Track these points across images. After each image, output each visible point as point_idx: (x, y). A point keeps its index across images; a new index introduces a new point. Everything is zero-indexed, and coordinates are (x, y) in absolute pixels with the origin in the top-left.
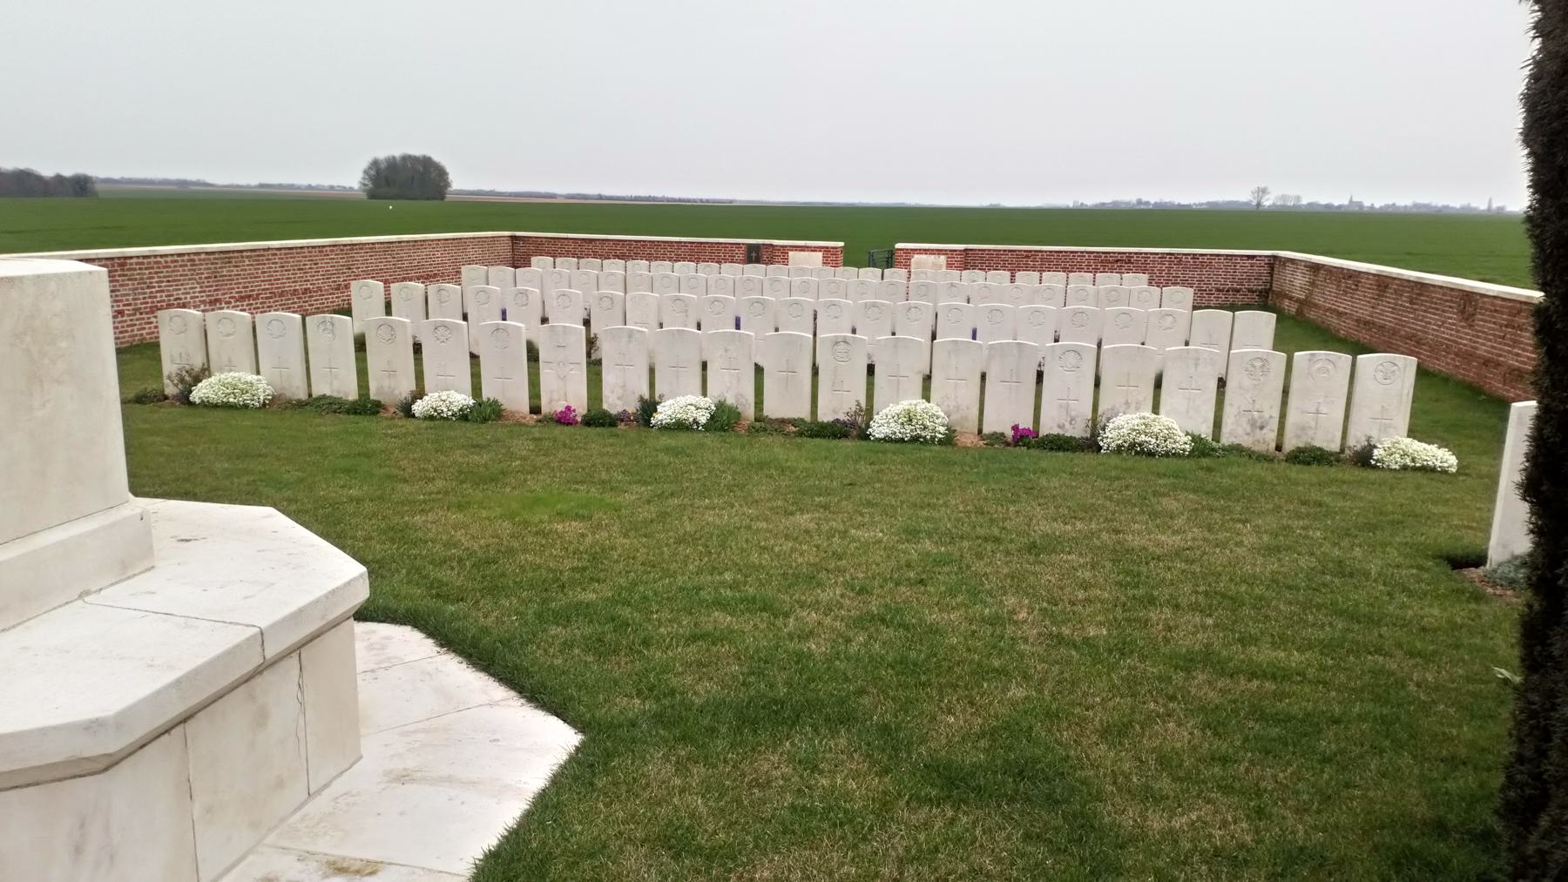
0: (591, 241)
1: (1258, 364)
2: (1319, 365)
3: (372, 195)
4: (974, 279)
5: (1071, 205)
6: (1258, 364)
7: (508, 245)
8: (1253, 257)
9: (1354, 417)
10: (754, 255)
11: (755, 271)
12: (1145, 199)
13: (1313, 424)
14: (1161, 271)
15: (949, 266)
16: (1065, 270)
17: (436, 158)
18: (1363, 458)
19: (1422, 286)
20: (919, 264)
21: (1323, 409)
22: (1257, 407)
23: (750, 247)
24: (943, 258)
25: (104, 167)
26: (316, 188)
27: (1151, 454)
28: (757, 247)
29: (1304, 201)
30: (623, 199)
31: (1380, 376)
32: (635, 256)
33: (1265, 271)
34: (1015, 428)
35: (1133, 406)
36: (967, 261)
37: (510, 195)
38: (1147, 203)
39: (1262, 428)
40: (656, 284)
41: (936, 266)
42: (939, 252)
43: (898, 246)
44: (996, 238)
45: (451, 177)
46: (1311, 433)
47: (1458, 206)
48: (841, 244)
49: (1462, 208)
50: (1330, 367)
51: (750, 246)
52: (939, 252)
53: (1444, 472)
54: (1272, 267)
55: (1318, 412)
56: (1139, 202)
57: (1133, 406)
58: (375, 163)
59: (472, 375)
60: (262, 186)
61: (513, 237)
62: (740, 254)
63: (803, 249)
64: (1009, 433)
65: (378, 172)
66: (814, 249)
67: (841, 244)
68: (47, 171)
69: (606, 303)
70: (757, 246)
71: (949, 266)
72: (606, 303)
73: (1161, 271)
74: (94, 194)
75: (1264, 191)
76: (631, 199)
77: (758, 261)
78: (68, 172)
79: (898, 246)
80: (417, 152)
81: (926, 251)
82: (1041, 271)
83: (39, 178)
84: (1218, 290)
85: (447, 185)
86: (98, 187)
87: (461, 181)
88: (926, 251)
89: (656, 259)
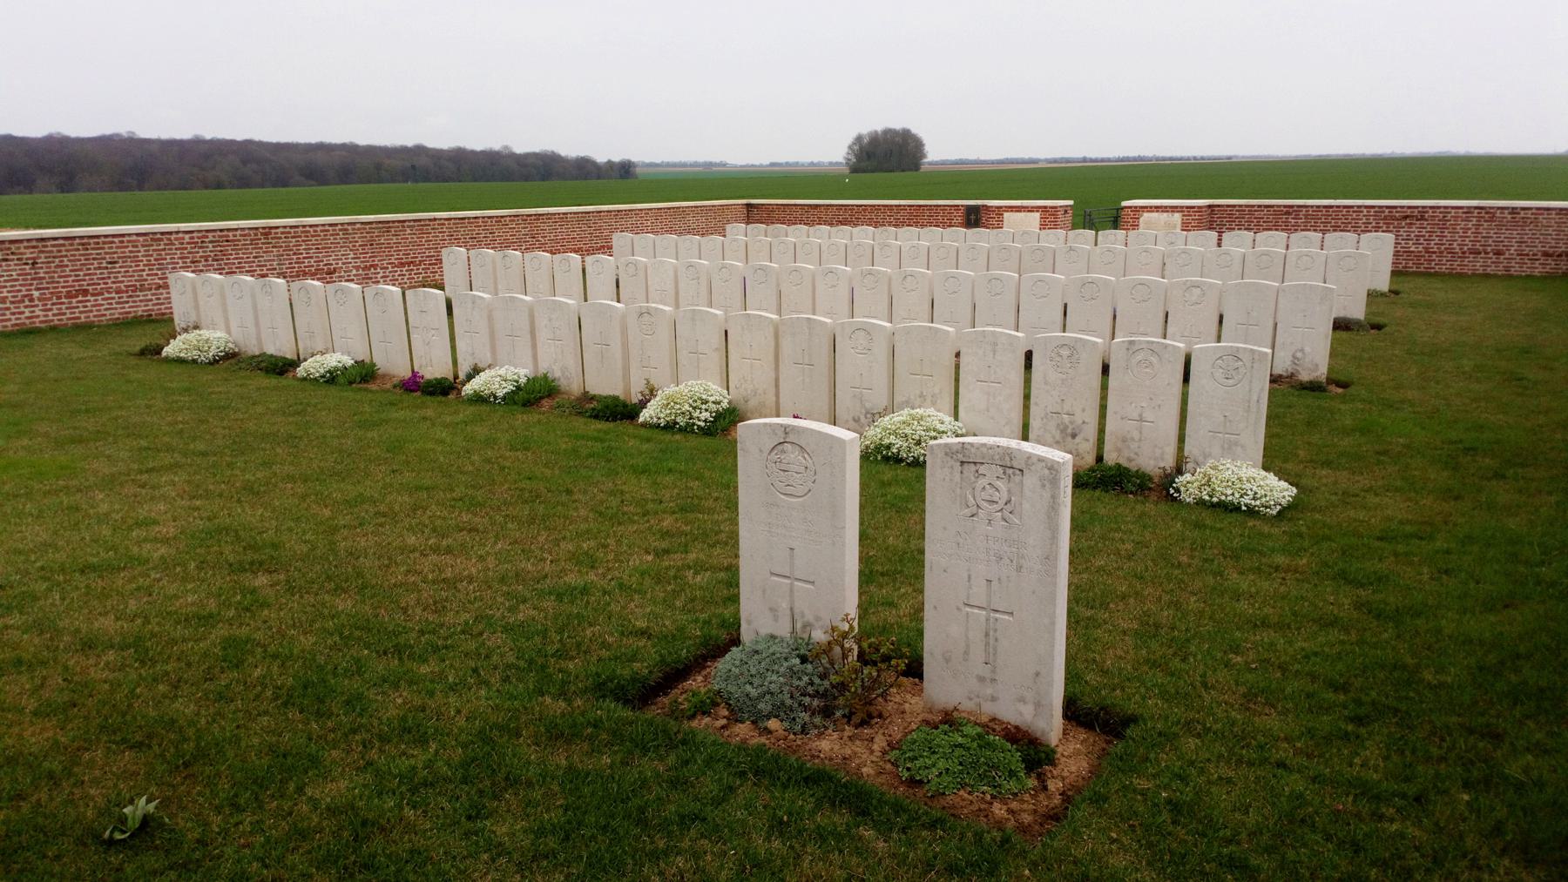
0: (817, 206)
1: (1065, 352)
2: (1140, 356)
3: (855, 170)
4: (1238, 242)
6: (1065, 352)
7: (1205, 214)
10: (973, 218)
13: (1136, 435)
14: (1466, 230)
15: (1186, 227)
16: (1355, 229)
17: (914, 131)
20: (1149, 226)
21: (1148, 415)
22: (1067, 408)
24: (1177, 217)
25: (569, 147)
26: (819, 164)
27: (898, 460)
30: (1109, 160)
31: (1219, 374)
35: (929, 400)
36: (1215, 221)
37: (993, 162)
39: (1074, 436)
41: (1169, 226)
42: (1174, 209)
43: (1124, 204)
45: (928, 148)
46: (1134, 446)
48: (1071, 202)
50: (1154, 359)
55: (1141, 420)
57: (929, 400)
58: (859, 139)
60: (773, 164)
61: (748, 205)
63: (1019, 209)
65: (861, 148)
67: (1071, 202)
68: (601, 158)
69: (631, 270)
71: (1186, 227)
72: (631, 270)
73: (1466, 230)
74: (634, 176)
76: (1135, 159)
78: (616, 159)
79: (1124, 204)
80: (897, 125)
81: (1158, 208)
82: (1324, 232)
83: (594, 163)
84: (1546, 254)
85: (923, 156)
86: (638, 170)
87: (938, 150)
88: (1158, 208)
89: (1336, 228)
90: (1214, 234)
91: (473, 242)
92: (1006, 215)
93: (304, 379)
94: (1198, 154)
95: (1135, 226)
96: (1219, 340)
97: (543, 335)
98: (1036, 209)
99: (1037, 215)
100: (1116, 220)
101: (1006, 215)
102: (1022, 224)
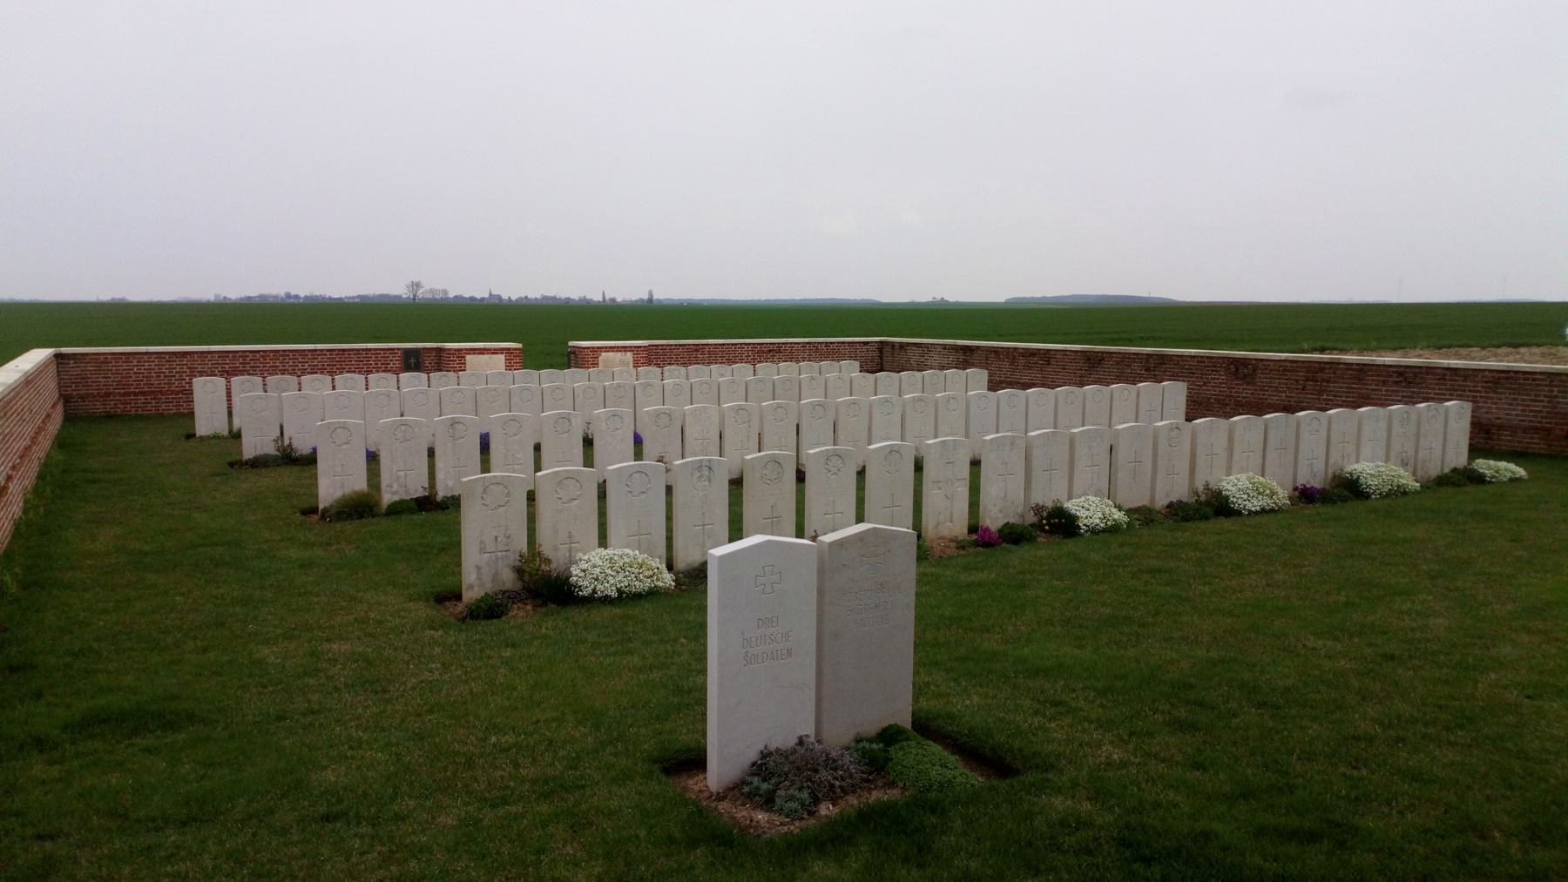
0: (185, 354)
4: (674, 375)
5: (212, 298)
9: (678, 514)
10: (413, 362)
11: (412, 381)
18: (1060, 523)
19: (1163, 357)
32: (274, 371)
33: (876, 354)
34: (619, 590)
36: (652, 357)
38: (297, 297)
40: (515, 399)
41: (623, 363)
42: (625, 349)
44: (887, 339)
48: (520, 346)
51: (407, 352)
52: (625, 349)
53: (653, 593)
54: (881, 350)
62: (396, 363)
67: (520, 346)
70: (417, 351)
81: (612, 349)
88: (612, 349)
90: (258, 379)
91: (230, 367)
92: (468, 357)
93: (359, 508)
94: (1038, 294)
95: (596, 365)
96: (538, 468)
97: (1081, 464)
98: (501, 351)
99: (502, 357)
100: (573, 359)
101: (468, 357)
102: (487, 366)
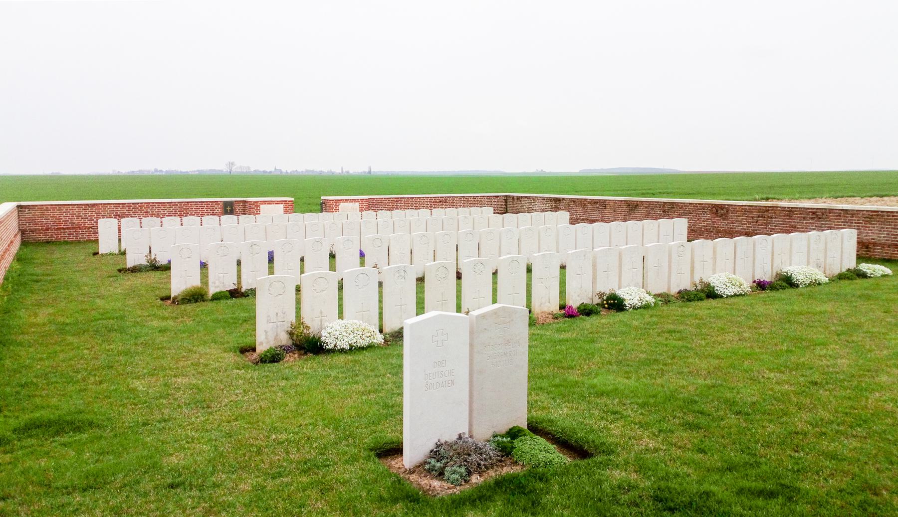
8: (497, 197)
12: (159, 169)
16: (389, 210)
23: (226, 204)
24: (357, 204)
28: (231, 204)
29: (252, 170)
33: (503, 203)
34: (350, 345)
42: (354, 200)
47: (577, 171)
49: (580, 172)
53: (370, 347)
54: (506, 201)
56: (156, 171)
59: (565, 283)
63: (270, 203)
64: (348, 348)
66: (278, 203)
75: (233, 164)
77: (232, 212)
